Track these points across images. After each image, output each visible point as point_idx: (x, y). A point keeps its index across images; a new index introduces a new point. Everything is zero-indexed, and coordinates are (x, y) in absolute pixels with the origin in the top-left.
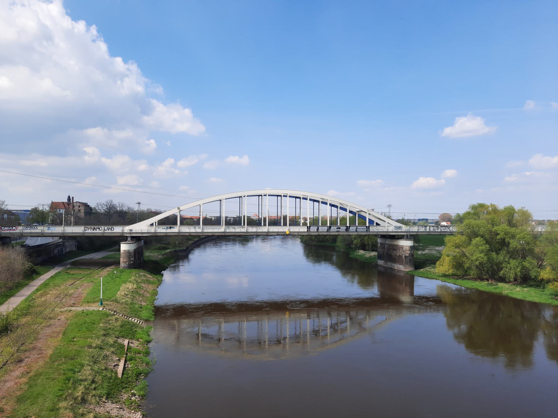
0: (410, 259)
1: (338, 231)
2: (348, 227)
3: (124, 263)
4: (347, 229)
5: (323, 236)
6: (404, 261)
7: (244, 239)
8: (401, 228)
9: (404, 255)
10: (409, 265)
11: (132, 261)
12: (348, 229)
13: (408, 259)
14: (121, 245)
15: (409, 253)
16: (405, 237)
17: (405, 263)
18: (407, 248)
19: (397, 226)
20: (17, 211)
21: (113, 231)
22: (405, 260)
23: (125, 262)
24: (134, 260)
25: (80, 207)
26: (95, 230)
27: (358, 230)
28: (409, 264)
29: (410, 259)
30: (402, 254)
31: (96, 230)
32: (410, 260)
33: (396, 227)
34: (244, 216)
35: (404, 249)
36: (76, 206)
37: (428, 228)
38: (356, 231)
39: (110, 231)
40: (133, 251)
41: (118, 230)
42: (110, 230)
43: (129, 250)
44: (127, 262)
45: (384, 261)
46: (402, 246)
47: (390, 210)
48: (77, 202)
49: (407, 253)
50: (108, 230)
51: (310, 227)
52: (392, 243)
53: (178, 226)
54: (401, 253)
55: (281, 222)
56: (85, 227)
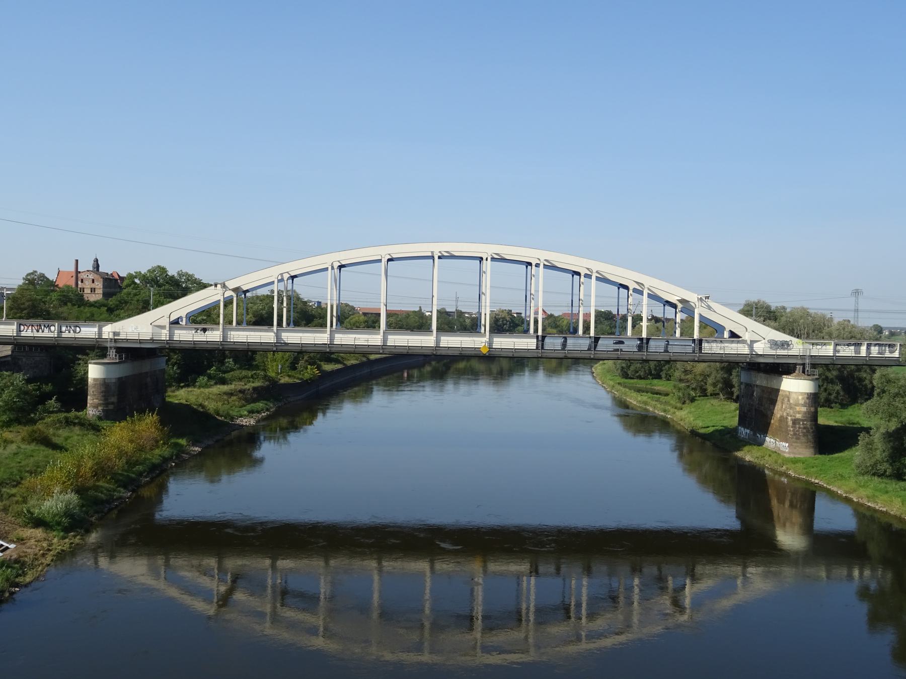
0: (804, 428)
2: (645, 341)
3: (94, 407)
6: (790, 430)
8: (788, 345)
9: (791, 416)
11: (113, 403)
13: (799, 428)
14: (90, 366)
15: (805, 413)
17: (792, 438)
18: (800, 397)
22: (793, 431)
23: (96, 407)
25: (95, 282)
26: (40, 331)
27: (670, 349)
28: (803, 439)
29: (804, 428)
30: (788, 415)
31: (43, 332)
32: (805, 431)
33: (775, 344)
34: (587, 315)
35: (791, 401)
38: (666, 351)
39: (72, 335)
41: (88, 332)
42: (72, 332)
43: (105, 379)
44: (100, 406)
45: (751, 430)
46: (788, 393)
47: (857, 303)
48: (88, 271)
49: (799, 412)
50: (67, 332)
51: (543, 337)
53: (382, 331)
54: (785, 410)
55: (430, 325)
56: (20, 324)
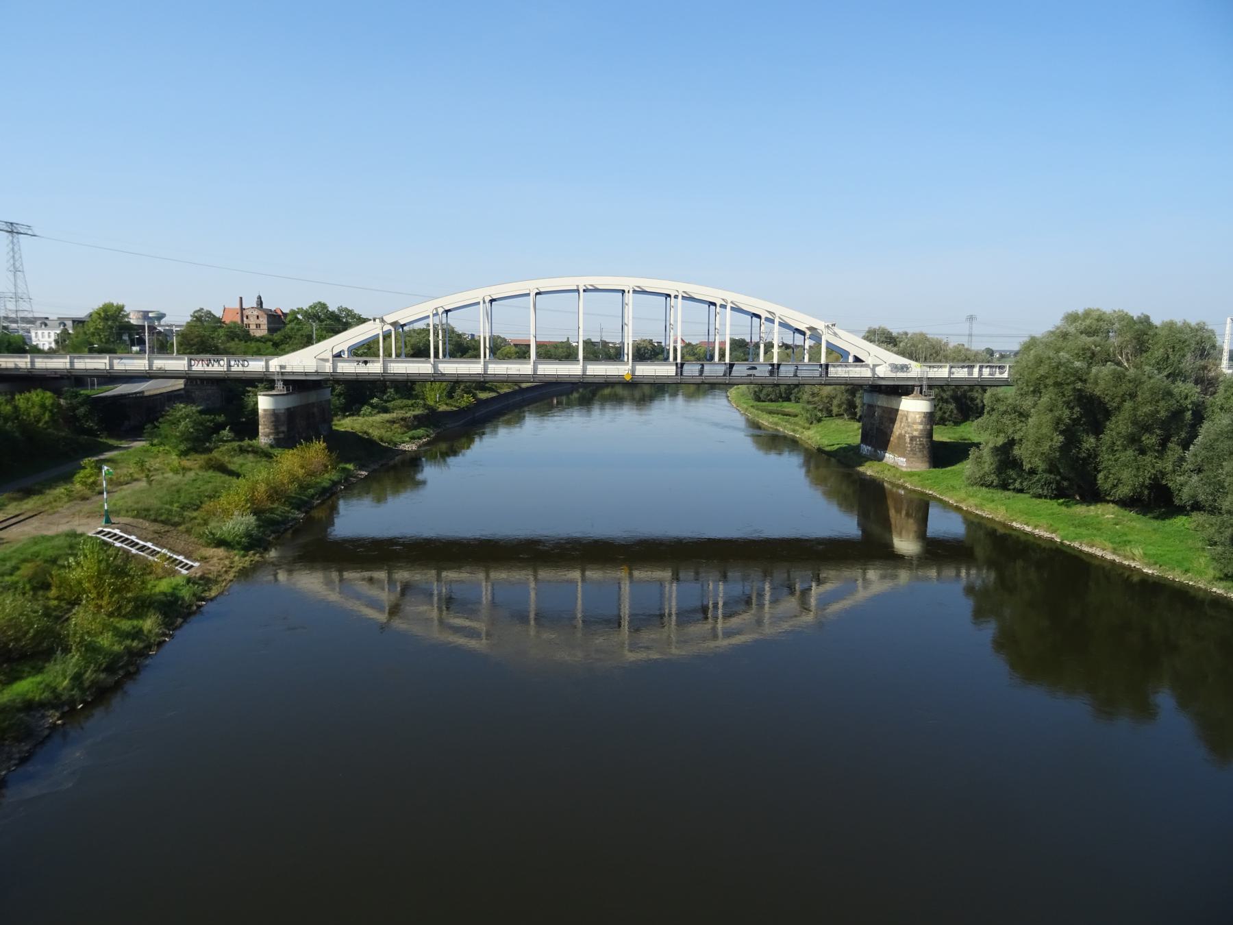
0: (921, 444)
1: (750, 375)
2: (776, 367)
3: (265, 436)
4: (775, 368)
5: (570, 386)
7: (655, 390)
9: (909, 433)
10: (918, 458)
11: (283, 432)
12: (776, 371)
15: (921, 430)
16: (917, 389)
18: (917, 416)
19: (897, 365)
20: (934, 334)
21: (246, 369)
22: (911, 447)
24: (288, 431)
26: (210, 365)
28: (919, 455)
29: (921, 444)
31: (213, 366)
32: (921, 447)
33: (895, 368)
35: (909, 420)
36: (253, 316)
37: (976, 371)
38: (796, 375)
40: (283, 411)
41: (255, 366)
46: (906, 413)
47: (971, 328)
49: (916, 430)
51: (682, 365)
52: (889, 406)
54: (903, 428)
